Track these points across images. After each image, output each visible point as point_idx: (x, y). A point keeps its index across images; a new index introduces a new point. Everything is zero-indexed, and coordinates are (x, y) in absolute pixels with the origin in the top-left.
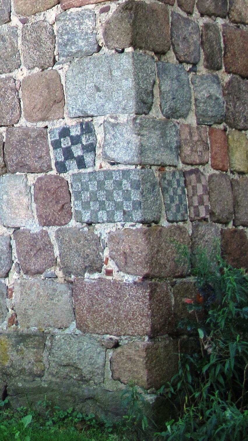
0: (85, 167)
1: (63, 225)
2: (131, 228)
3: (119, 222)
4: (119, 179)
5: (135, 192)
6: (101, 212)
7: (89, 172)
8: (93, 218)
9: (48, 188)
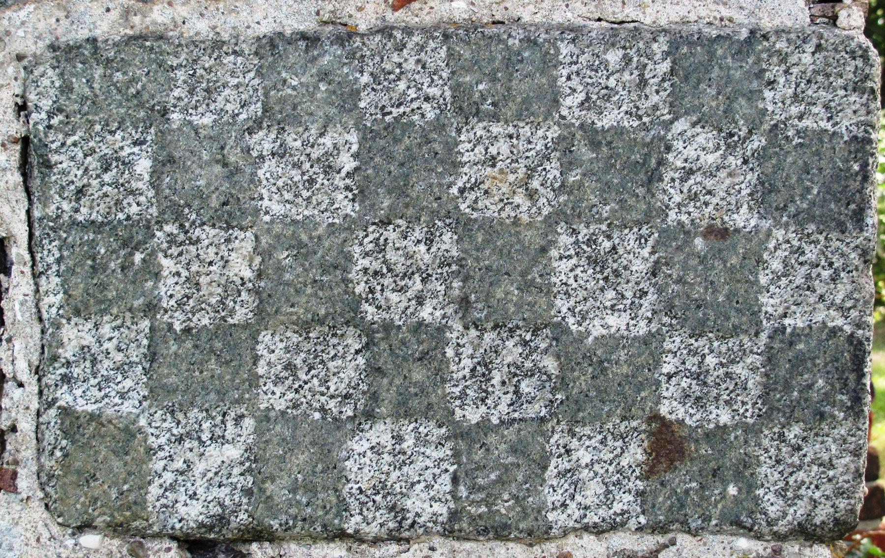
3: (588, 539)
5: (811, 253)
7: (266, 28)
8: (278, 490)
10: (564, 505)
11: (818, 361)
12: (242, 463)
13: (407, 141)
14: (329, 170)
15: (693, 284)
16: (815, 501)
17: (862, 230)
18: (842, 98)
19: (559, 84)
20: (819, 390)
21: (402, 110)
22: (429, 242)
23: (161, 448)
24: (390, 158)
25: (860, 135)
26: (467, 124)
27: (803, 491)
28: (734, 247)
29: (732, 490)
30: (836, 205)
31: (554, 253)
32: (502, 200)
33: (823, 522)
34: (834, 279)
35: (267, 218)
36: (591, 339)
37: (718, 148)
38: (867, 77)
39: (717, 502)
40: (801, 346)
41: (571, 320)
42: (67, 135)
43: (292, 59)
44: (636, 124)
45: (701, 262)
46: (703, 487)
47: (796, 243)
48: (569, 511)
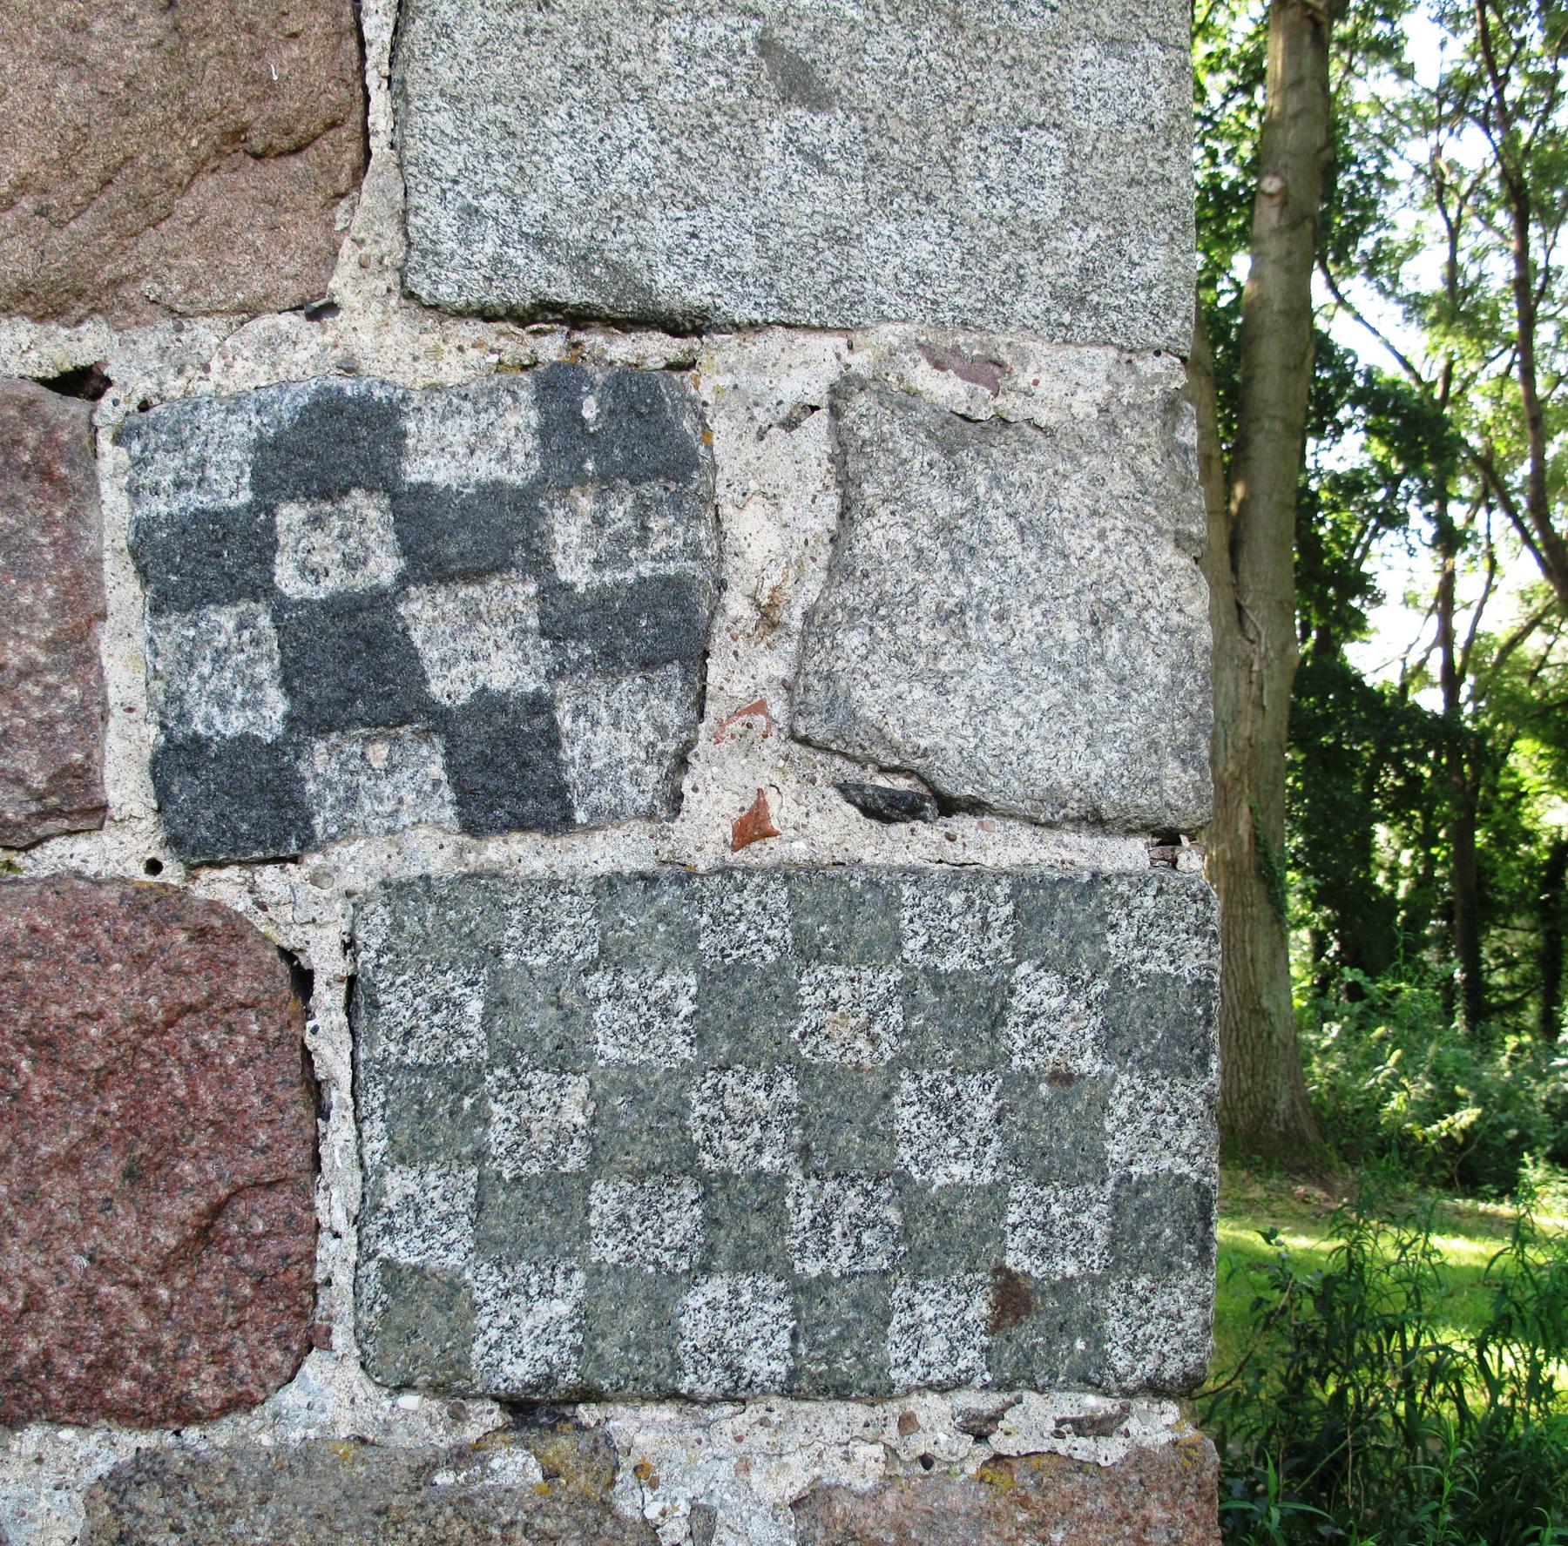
2: (1082, 1448)
10: (907, 1363)
14: (666, 1013)
23: (486, 1303)
27: (1151, 1345)
31: (897, 1100)
35: (602, 1063)
40: (1148, 1195)
41: (914, 1169)
42: (397, 974)
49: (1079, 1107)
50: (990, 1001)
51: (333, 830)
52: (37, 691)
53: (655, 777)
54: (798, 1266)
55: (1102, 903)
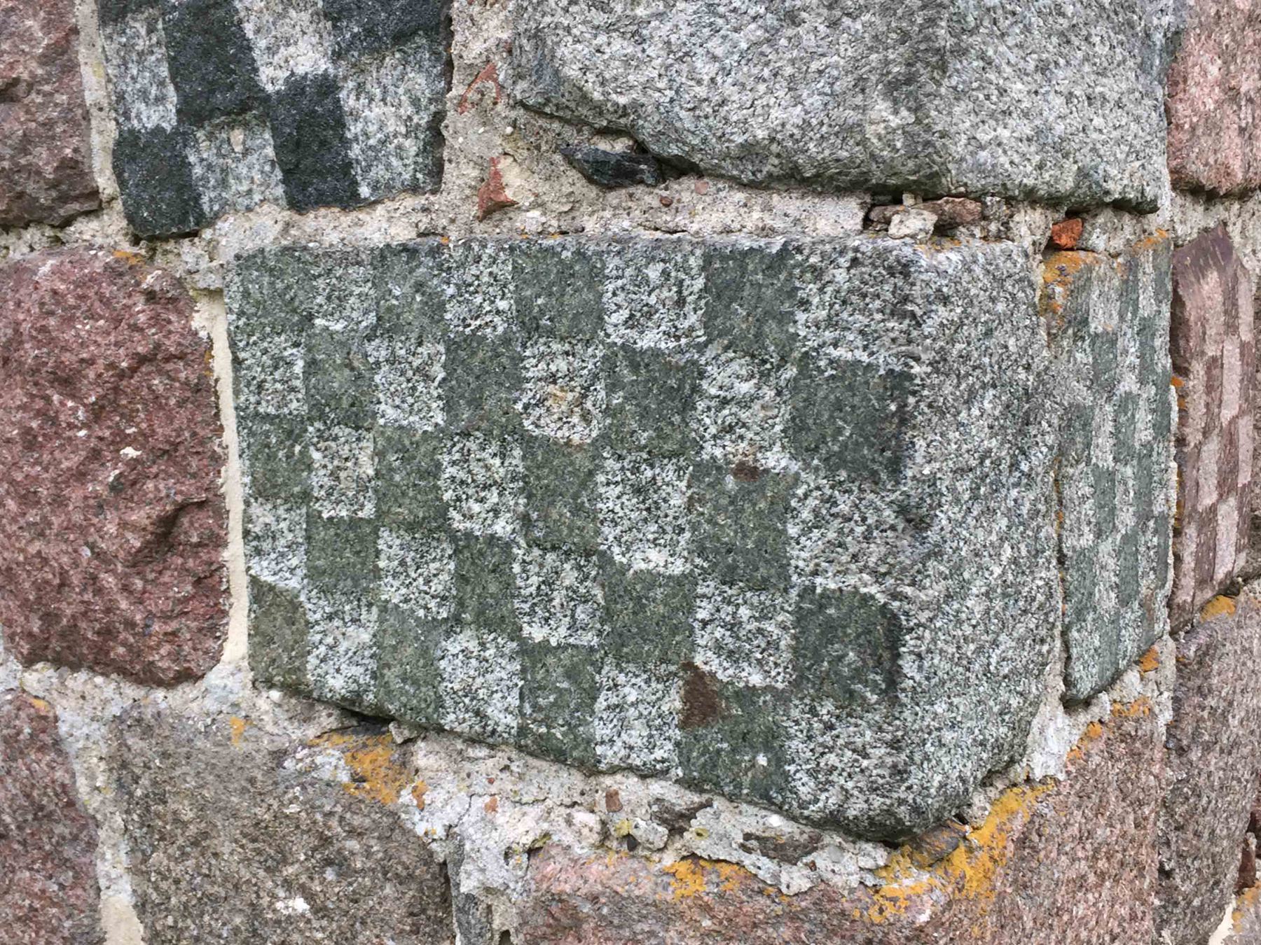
0: (349, 200)
1: (160, 683)
2: (765, 867)
3: (633, 780)
4: (666, 345)
6: (465, 640)
8: (391, 675)
9: (59, 364)
10: (612, 741)
11: (849, 631)
12: (371, 647)
13: (481, 354)
14: (428, 378)
15: (722, 526)
16: (847, 791)
17: (898, 483)
18: (879, 322)
19: (604, 300)
20: (849, 664)
21: (478, 322)
22: (503, 457)
23: (317, 623)
24: (469, 371)
25: (897, 369)
26: (530, 339)
27: (834, 777)
28: (762, 488)
29: (762, 760)
30: (869, 450)
31: (601, 478)
32: (560, 419)
33: (856, 817)
34: (867, 538)
35: (382, 421)
36: (631, 571)
37: (752, 376)
38: (906, 299)
39: (747, 770)
40: (831, 611)
41: (616, 550)
42: (249, 336)
43: (397, 269)
44: (671, 345)
45: (732, 503)
46: (734, 750)
47: (828, 492)
48: (615, 748)
49: (762, 505)
50: (681, 382)
51: (216, 208)
52: (39, 100)
53: (413, 151)
54: (526, 629)
55: (791, 274)
